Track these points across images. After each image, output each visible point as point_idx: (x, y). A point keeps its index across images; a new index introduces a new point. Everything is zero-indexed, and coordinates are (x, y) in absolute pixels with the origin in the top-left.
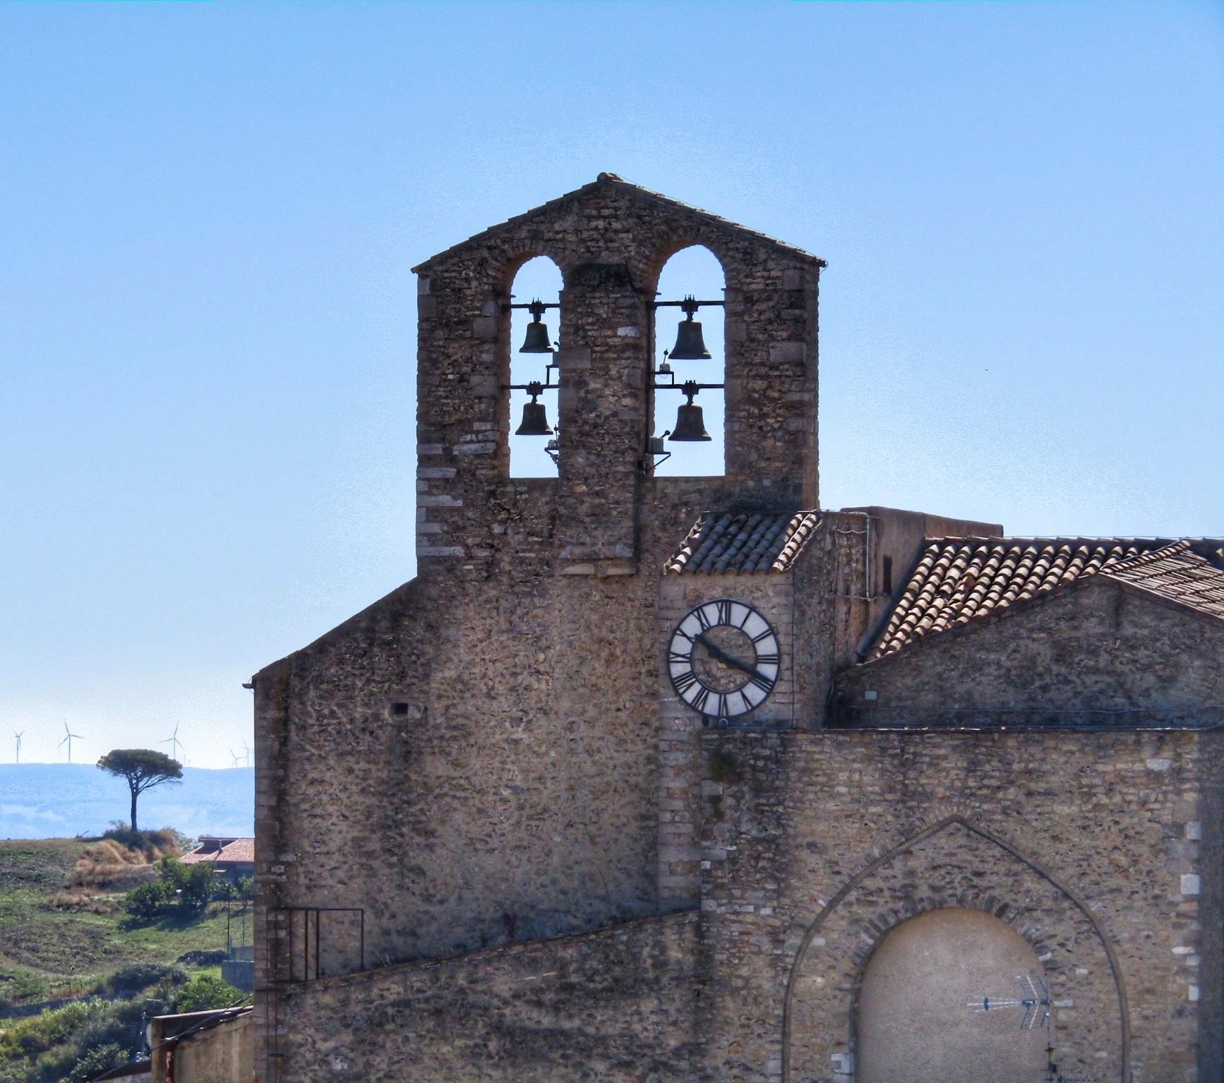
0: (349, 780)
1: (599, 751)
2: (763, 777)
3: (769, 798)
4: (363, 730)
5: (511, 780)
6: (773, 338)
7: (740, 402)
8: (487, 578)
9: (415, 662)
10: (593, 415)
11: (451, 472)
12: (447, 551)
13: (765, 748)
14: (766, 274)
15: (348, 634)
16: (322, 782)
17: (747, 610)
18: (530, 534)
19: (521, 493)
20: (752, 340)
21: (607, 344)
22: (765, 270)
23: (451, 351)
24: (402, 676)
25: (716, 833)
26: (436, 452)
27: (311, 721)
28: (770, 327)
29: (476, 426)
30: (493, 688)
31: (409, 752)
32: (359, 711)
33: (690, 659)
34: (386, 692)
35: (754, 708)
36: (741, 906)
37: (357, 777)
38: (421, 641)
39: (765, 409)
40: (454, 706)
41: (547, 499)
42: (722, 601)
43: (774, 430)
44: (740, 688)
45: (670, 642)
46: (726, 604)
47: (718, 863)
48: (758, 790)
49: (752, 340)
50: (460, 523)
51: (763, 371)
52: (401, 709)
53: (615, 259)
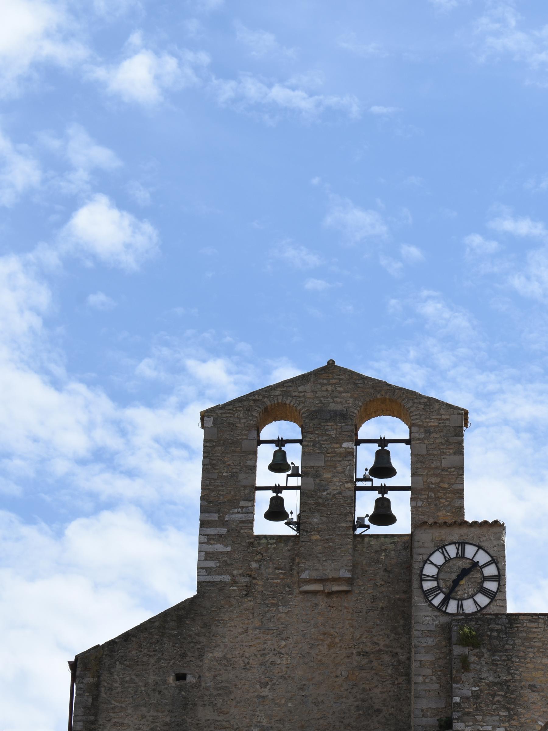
0: (142, 723)
1: (323, 702)
2: (496, 642)
3: (501, 656)
4: (154, 690)
5: (259, 722)
6: (444, 453)
7: (422, 490)
8: (246, 595)
9: (193, 648)
10: (325, 493)
11: (223, 531)
12: (218, 578)
13: (498, 624)
14: (439, 417)
15: (146, 629)
16: (122, 725)
17: (476, 548)
18: (276, 569)
19: (271, 544)
20: (430, 455)
21: (335, 452)
22: (438, 414)
23: (226, 459)
24: (183, 656)
25: (464, 678)
26: (213, 519)
27: (115, 685)
28: (442, 447)
29: (242, 503)
30: (248, 663)
31: (187, 704)
32: (151, 679)
33: (436, 578)
34: (171, 666)
35: (482, 609)
36: (482, 726)
37: (148, 721)
38: (198, 634)
39: (439, 494)
40: (220, 674)
41: (289, 548)
42: (459, 543)
43: (445, 506)
44: (472, 597)
45: (422, 569)
46: (461, 544)
47: (465, 699)
48: (493, 651)
49: (430, 455)
50: (228, 562)
51: (438, 472)
52: (181, 677)
53: (339, 407)
